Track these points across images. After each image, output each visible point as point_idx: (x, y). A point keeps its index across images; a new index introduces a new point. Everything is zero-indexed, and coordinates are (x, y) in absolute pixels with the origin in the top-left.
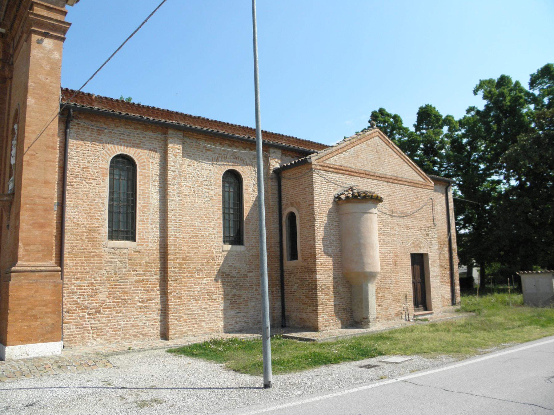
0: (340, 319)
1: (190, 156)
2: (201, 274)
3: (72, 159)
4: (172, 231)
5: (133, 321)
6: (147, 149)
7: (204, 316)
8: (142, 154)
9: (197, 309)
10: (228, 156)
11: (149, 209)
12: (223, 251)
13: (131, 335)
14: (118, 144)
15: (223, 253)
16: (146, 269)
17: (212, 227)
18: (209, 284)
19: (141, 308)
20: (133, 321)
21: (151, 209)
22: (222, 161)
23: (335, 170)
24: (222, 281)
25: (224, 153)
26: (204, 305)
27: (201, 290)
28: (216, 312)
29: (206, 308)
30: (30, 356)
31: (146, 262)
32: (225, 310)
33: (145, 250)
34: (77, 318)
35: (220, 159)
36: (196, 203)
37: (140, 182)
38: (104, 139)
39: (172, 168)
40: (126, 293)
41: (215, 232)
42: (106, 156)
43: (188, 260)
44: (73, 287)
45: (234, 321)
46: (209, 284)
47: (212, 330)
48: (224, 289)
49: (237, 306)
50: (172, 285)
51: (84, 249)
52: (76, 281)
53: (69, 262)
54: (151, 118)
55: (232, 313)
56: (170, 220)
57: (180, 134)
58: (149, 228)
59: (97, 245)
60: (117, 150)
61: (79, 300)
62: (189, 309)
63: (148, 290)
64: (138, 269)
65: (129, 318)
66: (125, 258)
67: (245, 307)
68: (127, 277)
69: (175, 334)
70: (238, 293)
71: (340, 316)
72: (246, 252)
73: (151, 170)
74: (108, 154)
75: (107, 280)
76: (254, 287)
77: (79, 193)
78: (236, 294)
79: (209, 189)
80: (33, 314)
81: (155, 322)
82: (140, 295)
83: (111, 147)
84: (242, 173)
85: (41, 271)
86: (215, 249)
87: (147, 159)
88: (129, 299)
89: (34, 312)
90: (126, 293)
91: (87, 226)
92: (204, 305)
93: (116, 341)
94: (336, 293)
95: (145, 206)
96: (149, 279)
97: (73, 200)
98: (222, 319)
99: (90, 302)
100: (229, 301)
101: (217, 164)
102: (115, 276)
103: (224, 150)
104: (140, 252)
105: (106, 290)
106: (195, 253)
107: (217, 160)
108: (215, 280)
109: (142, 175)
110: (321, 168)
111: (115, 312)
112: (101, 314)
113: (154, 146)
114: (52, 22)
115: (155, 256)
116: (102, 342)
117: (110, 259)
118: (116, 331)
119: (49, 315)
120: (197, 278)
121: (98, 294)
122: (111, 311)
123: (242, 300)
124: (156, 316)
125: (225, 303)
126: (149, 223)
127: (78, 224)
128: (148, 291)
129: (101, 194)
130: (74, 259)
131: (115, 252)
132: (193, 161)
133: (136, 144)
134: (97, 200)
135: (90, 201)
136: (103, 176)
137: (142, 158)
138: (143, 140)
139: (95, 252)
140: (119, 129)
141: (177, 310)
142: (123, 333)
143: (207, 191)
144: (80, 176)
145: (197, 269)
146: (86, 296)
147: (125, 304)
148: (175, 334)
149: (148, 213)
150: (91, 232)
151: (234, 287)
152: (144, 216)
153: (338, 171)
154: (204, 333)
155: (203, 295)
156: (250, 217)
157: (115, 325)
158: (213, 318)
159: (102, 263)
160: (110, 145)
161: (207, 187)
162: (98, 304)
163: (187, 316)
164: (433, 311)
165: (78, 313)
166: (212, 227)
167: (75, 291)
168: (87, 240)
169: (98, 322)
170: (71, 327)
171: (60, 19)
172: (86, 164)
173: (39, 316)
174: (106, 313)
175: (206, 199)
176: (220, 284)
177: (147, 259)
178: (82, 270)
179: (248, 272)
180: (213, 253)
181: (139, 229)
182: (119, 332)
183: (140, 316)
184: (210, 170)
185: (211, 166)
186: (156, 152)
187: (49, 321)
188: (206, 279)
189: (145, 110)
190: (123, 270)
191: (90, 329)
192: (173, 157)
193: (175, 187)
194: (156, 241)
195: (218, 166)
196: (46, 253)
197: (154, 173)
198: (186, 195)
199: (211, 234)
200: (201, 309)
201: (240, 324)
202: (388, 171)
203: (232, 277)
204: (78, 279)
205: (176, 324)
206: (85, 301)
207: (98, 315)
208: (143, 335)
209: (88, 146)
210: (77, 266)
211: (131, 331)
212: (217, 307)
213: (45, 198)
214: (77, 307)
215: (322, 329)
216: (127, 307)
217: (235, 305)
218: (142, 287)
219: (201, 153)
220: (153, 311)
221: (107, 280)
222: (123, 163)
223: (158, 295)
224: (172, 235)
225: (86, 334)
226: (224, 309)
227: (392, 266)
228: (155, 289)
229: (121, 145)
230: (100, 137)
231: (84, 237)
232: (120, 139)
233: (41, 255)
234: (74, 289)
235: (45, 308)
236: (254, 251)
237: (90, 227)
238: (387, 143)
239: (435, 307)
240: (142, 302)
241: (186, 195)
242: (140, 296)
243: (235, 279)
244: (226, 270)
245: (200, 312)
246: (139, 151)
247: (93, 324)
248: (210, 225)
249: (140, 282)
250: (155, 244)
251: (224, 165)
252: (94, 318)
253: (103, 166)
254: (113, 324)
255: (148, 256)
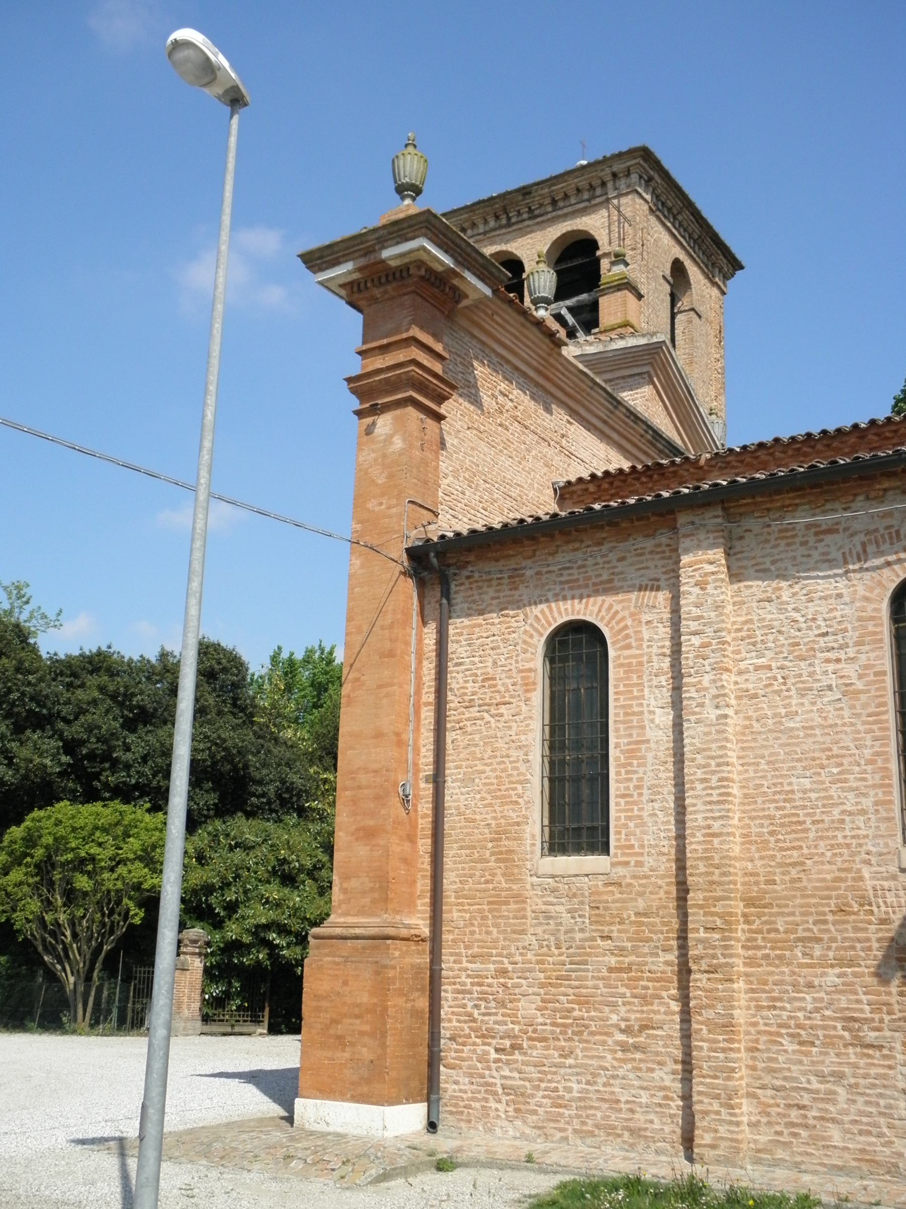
2: (817, 953)
3: (460, 664)
4: (699, 816)
5: (604, 1085)
6: (631, 589)
7: (834, 1102)
8: (617, 607)
9: (804, 1073)
11: (644, 757)
13: (597, 1126)
14: (557, 597)
16: (637, 932)
17: (852, 789)
19: (625, 1047)
20: (604, 1085)
21: (650, 755)
22: (881, 553)
25: (887, 522)
27: (817, 1010)
28: (881, 1095)
30: (331, 1129)
31: (638, 914)
33: (634, 877)
34: (471, 1059)
35: (871, 549)
36: (791, 715)
37: (616, 686)
38: (525, 597)
39: (694, 626)
40: (584, 1001)
42: (531, 636)
43: (770, 905)
44: (463, 979)
50: (703, 983)
51: (487, 882)
52: (470, 962)
53: (455, 915)
56: (692, 782)
57: (713, 517)
58: (645, 814)
59: (516, 871)
60: (556, 615)
61: (476, 1012)
62: (774, 1070)
63: (644, 997)
64: (614, 935)
65: (594, 1075)
66: (582, 903)
68: (589, 955)
69: (713, 1147)
73: (645, 645)
74: (536, 630)
75: (538, 962)
77: (476, 745)
79: (838, 661)
80: (339, 1033)
81: (666, 1098)
82: (623, 1009)
83: (542, 612)
85: (357, 937)
86: (868, 863)
87: (632, 615)
88: (592, 1019)
89: (340, 1029)
90: (584, 1001)
91: (493, 823)
93: (559, 1135)
95: (632, 751)
96: (646, 964)
97: (464, 764)
99: (500, 1018)
101: (861, 570)
102: (556, 952)
103: (889, 514)
104: (620, 885)
105: (536, 990)
106: (793, 881)
107: (864, 555)
109: (622, 665)
111: (556, 1054)
112: (525, 1054)
113: (652, 573)
114: (382, 376)
115: (662, 894)
116: (528, 1131)
117: (544, 908)
118: (560, 1106)
119: (366, 1039)
120: (800, 965)
121: (519, 1000)
122: (547, 1048)
124: (667, 1077)
126: (645, 798)
127: (474, 820)
128: (645, 1000)
129: (523, 737)
130: (466, 907)
131: (557, 886)
132: (774, 584)
133: (602, 583)
134: (514, 753)
135: (499, 759)
136: (527, 691)
137: (619, 617)
138: (621, 566)
139: (510, 889)
140: (559, 557)
141: (716, 1069)
142: (578, 1116)
143: (831, 667)
144: (477, 702)
145: (801, 934)
146: (493, 1004)
147: (580, 1033)
148: (713, 1147)
149: (641, 770)
150: (500, 839)
152: (631, 780)
155: (824, 1028)
157: (556, 1090)
158: (870, 1115)
159: (524, 917)
160: (540, 607)
162: (517, 1028)
163: (770, 1092)
165: (474, 1044)
166: (852, 789)
167: (469, 987)
168: (493, 858)
169: (516, 1075)
170: (461, 1079)
171: (392, 363)
172: (489, 670)
173: (348, 1039)
174: (535, 1053)
175: (830, 696)
177: (641, 904)
178: (483, 937)
180: (861, 879)
181: (618, 819)
182: (567, 1112)
183: (621, 1072)
184: (839, 596)
185: (842, 583)
186: (658, 589)
187: (366, 1054)
188: (837, 970)
190: (578, 936)
191: (500, 1091)
192: (697, 590)
193: (706, 680)
194: (665, 850)
195: (867, 575)
196: (376, 895)
197: (655, 650)
198: (755, 696)
199: (850, 814)
204: (473, 958)
205: (718, 1113)
206: (489, 1014)
207: (517, 1056)
208: (632, 1131)
209: (493, 624)
210: (473, 925)
211: (599, 1114)
212: (884, 1077)
213: (376, 771)
214: (471, 1028)
216: (587, 1041)
218: (627, 986)
219: (802, 550)
220: (660, 1063)
221: (538, 962)
222: (577, 644)
223: (673, 1013)
224: (699, 828)
225: (493, 1104)
228: (664, 994)
229: (565, 598)
230: (516, 593)
231: (488, 853)
232: (561, 583)
233: (368, 900)
234: (464, 984)
235: (358, 1021)
237: (498, 825)
240: (627, 1031)
241: (755, 696)
242: (623, 1014)
245: (815, 1085)
246: (609, 599)
247: (505, 1077)
248: (846, 781)
249: (620, 970)
250: (664, 859)
251: (888, 564)
252: (508, 1063)
253: (527, 666)
254: (554, 1085)
255: (641, 894)
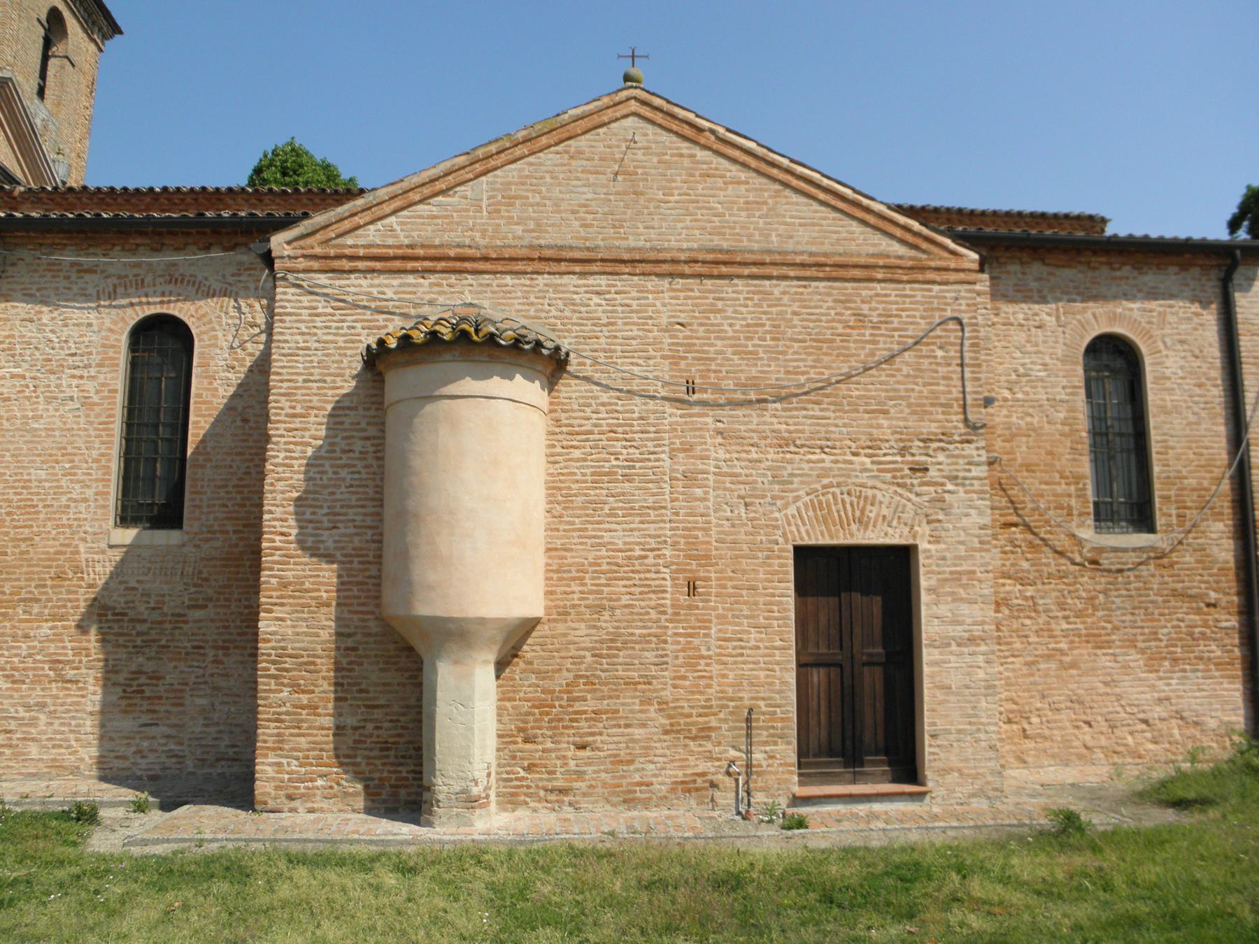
0: (358, 776)
1: (31, 295)
9: (13, 705)
10: (149, 279)
12: (111, 547)
15: (110, 552)
17: (79, 481)
18: (58, 638)
22: (127, 295)
23: (378, 265)
24: (101, 632)
26: (37, 695)
27: (30, 655)
28: (73, 718)
29: (44, 705)
32: (106, 712)
35: (120, 290)
36: (37, 418)
41: (90, 493)
45: (133, 749)
46: (58, 638)
47: (58, 768)
48: (107, 653)
49: (146, 705)
54: (125, 214)
55: (128, 724)
67: (174, 709)
70: (150, 667)
71: (363, 767)
72: (185, 550)
76: (211, 653)
78: (144, 669)
79: (81, 377)
84: (190, 322)
86: (84, 540)
92: (37, 695)
94: (346, 687)
98: (93, 739)
100: (119, 689)
101: (110, 306)
103: (138, 265)
106: (22, 553)
107: (112, 295)
108: (78, 627)
110: (315, 265)
120: (21, 621)
123: (162, 689)
125: (105, 694)
132: (37, 308)
143: (75, 382)
151: (138, 650)
153: (397, 264)
154: (34, 775)
155: (34, 669)
156: (210, 444)
158: (63, 733)
161: (76, 372)
164: (930, 785)
166: (79, 481)
176: (93, 638)
179: (189, 607)
180: (78, 552)
184: (90, 325)
188: (50, 624)
189: (148, 200)
195: (114, 311)
199: (75, 501)
200: (28, 707)
201: (152, 758)
202: (681, 235)
203: (132, 620)
215: (271, 804)
217: (138, 701)
219: (65, 283)
226: (102, 712)
227: (672, 594)
236: (218, 544)
238: (687, 131)
239: (946, 771)
243: (144, 627)
244: (118, 601)
245: (22, 714)
248: (75, 474)
251: (132, 305)
